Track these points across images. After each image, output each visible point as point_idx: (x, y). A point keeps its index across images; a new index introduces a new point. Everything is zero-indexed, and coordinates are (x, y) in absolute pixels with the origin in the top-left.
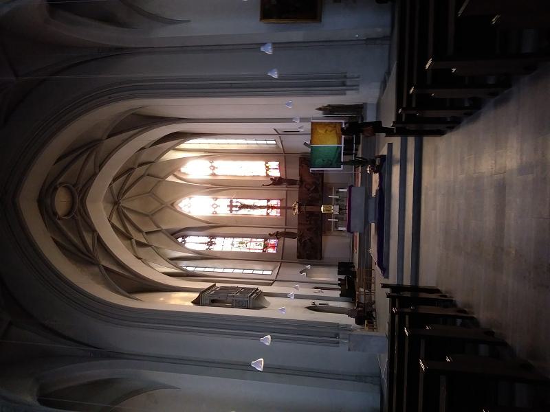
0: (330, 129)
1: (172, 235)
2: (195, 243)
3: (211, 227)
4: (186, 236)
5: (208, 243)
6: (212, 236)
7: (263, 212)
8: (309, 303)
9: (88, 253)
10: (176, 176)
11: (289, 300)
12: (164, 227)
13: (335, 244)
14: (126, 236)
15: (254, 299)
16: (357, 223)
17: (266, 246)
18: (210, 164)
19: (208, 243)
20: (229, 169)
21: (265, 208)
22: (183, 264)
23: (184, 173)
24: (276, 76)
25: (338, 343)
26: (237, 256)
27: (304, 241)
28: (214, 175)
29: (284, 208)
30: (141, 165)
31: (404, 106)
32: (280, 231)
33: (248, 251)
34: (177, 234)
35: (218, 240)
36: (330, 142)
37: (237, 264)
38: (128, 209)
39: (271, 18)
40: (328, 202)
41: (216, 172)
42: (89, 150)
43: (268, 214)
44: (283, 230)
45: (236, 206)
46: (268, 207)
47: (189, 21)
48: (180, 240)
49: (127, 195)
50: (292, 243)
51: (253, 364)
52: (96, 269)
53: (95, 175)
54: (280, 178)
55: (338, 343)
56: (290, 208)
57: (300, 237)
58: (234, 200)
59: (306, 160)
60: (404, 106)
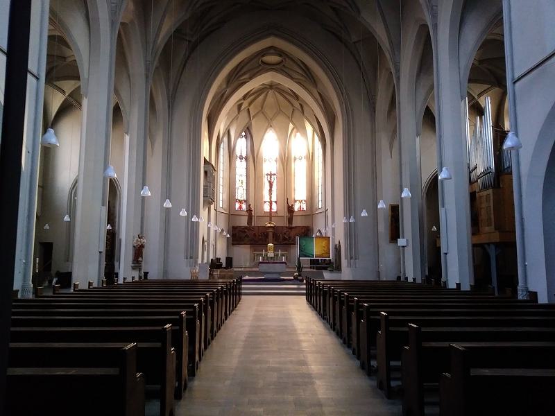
1: (248, 128)
2: (241, 146)
3: (253, 158)
4: (246, 138)
5: (241, 156)
6: (246, 159)
7: (267, 198)
8: (206, 238)
9: (235, 80)
10: (293, 129)
12: (253, 122)
13: (243, 254)
15: (210, 199)
16: (264, 268)
17: (240, 202)
19: (241, 156)
21: (269, 201)
22: (226, 139)
23: (295, 136)
25: (187, 258)
27: (246, 232)
28: (295, 159)
29: (271, 215)
31: (391, 318)
32: (253, 213)
34: (248, 132)
36: (316, 249)
37: (227, 181)
38: (267, 95)
39: (392, 211)
40: (275, 249)
41: (297, 161)
42: (308, 78)
43: (265, 202)
46: (271, 203)
48: (244, 134)
50: (243, 222)
52: (224, 86)
53: (292, 78)
54: (293, 212)
56: (271, 220)
59: (306, 232)
60: (391, 318)
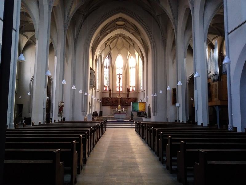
0: (144, 108)
1: (109, 54)
2: (107, 62)
3: (112, 67)
4: (109, 58)
6: (109, 68)
7: (118, 85)
8: (91, 103)
9: (104, 32)
10: (130, 54)
11: (93, 97)
12: (112, 51)
13: (107, 110)
14: (108, 40)
15: (92, 86)
16: (116, 116)
17: (106, 87)
18: (134, 67)
20: (132, 73)
21: (119, 86)
22: (100, 59)
24: (160, 93)
25: (82, 112)
26: (103, 78)
27: (108, 100)
28: (130, 68)
30: (133, 43)
32: (112, 91)
33: (104, 80)
34: (109, 56)
35: (108, 70)
36: (140, 108)
38: (117, 40)
40: (25, 122)
42: (136, 32)
43: (117, 87)
44: (112, 92)
45: (120, 76)
47: (173, 67)
48: (108, 56)
49: (123, 39)
50: (107, 96)
51: (74, 86)
53: (129, 32)
55: (82, 112)
56: (119, 95)
57: (110, 98)
58: (122, 76)
59: (135, 100)
